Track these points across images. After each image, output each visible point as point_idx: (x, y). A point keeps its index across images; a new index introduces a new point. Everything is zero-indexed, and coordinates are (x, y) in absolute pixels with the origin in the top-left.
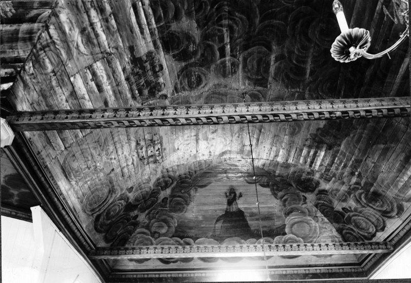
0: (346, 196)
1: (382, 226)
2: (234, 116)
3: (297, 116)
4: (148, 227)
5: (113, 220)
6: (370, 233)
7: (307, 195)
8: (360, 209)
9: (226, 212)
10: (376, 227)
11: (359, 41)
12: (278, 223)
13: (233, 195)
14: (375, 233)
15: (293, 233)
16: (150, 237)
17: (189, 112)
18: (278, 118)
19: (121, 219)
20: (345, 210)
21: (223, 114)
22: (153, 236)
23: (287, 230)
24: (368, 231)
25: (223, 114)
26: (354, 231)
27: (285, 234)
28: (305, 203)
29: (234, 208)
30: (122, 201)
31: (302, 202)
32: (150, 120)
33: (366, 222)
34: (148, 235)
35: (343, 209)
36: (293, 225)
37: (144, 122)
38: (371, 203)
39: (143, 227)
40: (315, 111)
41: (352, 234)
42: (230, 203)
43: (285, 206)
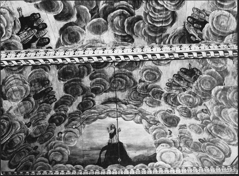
0: (200, 129)
1: (229, 152)
2: (92, 57)
3: (233, 52)
4: (47, 156)
5: (15, 150)
6: (221, 159)
7: (171, 129)
8: (211, 140)
9: (109, 143)
10: (224, 153)
11: (16, 50)
12: (152, 152)
13: (113, 130)
14: (224, 159)
15: (162, 160)
16: (48, 164)
17: (56, 54)
18: (128, 58)
19: (23, 148)
20: (201, 140)
21: (229, 49)
22: (50, 163)
23: (158, 158)
24: (220, 158)
25: (84, 55)
26: (210, 158)
27: (156, 161)
28: (171, 136)
29: (115, 140)
30: (22, 134)
31: (168, 136)
32: (24, 60)
33: (217, 150)
34: (47, 163)
35: (200, 140)
36: (162, 153)
37: (92, 58)
38: (218, 133)
39: (43, 156)
40: (220, 49)
41: (208, 161)
42: (112, 136)
43: (155, 139)
